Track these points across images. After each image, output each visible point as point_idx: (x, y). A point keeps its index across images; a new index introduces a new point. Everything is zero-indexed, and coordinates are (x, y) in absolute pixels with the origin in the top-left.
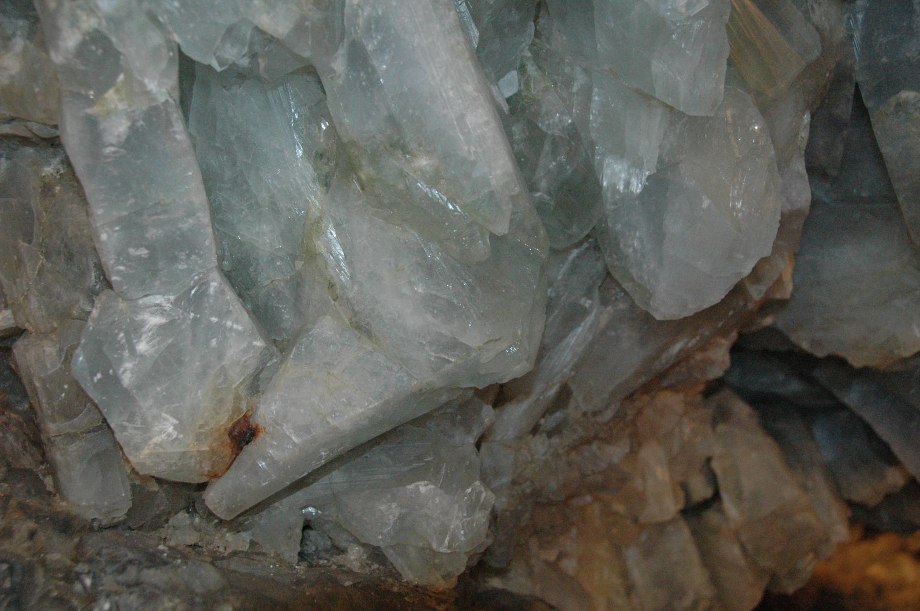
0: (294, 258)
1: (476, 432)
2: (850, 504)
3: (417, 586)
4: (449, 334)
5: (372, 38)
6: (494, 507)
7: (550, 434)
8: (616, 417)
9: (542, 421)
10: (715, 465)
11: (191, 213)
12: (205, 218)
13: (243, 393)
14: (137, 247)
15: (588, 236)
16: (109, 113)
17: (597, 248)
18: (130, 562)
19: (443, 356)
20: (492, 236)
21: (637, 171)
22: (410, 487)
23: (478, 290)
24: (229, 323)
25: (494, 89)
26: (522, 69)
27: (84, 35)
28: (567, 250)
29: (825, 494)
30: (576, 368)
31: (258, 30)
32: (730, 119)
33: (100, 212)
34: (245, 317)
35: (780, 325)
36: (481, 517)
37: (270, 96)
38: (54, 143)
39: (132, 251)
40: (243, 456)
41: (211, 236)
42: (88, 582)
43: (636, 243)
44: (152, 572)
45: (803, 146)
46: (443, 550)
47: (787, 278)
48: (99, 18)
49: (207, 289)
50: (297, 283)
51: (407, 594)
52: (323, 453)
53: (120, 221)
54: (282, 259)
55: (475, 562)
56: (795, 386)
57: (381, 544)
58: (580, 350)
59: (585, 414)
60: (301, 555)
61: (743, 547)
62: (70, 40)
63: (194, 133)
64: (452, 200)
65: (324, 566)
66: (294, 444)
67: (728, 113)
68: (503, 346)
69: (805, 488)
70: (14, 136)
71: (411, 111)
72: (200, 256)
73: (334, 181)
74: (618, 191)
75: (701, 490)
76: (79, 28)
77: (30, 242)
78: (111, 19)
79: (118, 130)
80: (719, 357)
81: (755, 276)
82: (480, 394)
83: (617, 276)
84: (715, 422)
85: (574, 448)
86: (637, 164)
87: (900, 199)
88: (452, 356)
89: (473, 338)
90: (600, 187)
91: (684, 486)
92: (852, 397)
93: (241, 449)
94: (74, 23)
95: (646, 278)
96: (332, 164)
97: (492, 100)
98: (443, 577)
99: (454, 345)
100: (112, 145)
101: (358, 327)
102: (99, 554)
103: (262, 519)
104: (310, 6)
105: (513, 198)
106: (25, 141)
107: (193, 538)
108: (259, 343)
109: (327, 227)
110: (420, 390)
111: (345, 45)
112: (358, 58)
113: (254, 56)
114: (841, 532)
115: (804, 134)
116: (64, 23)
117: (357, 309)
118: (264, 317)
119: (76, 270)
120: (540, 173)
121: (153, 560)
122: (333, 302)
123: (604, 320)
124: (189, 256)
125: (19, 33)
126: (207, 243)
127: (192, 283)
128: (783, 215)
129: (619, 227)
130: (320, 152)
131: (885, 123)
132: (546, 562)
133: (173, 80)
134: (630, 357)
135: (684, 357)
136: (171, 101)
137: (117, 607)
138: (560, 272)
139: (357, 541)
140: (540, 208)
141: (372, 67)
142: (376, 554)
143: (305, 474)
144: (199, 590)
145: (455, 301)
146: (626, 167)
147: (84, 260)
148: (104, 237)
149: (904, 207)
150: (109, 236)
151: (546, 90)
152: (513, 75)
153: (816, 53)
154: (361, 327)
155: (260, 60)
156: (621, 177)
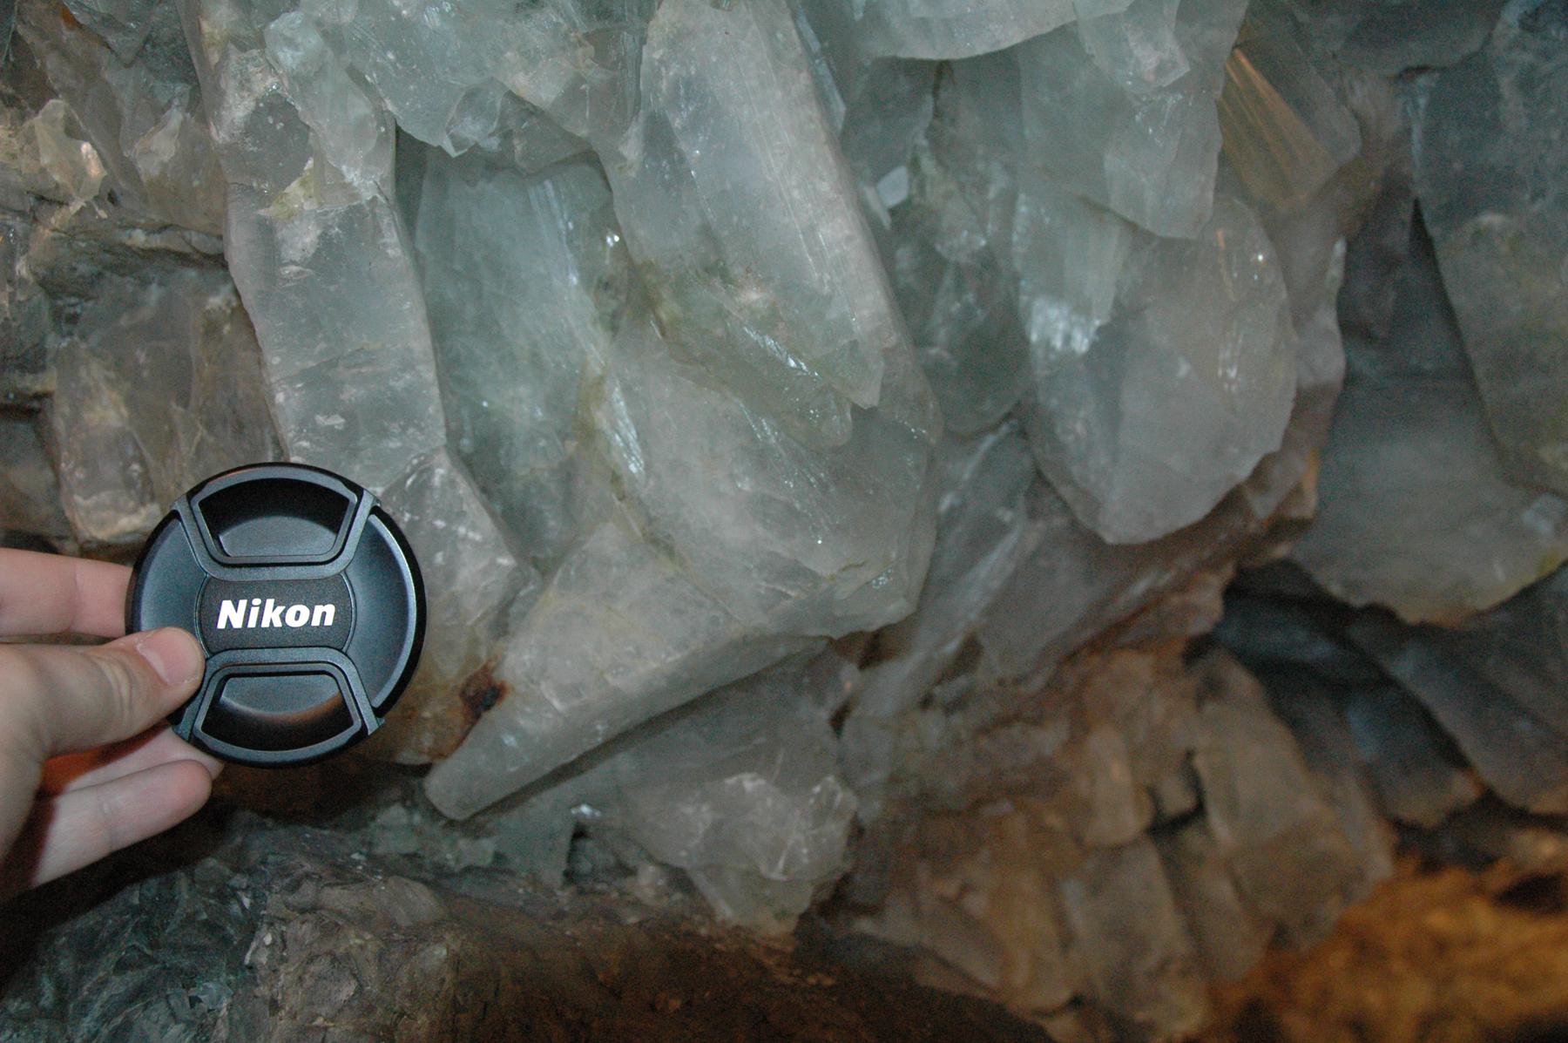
0: (564, 436)
1: (833, 702)
2: (1398, 825)
3: (738, 927)
4: (786, 554)
5: (680, 110)
6: (856, 816)
7: (950, 708)
8: (1048, 686)
9: (937, 690)
10: (1200, 762)
11: (408, 365)
12: (429, 373)
13: (482, 633)
14: (328, 414)
15: (1009, 416)
16: (291, 215)
17: (1023, 433)
18: (307, 876)
19: (779, 587)
20: (856, 409)
21: (1083, 320)
22: (731, 781)
23: (832, 489)
24: (462, 530)
25: (870, 194)
26: (915, 166)
27: (257, 101)
28: (979, 434)
29: (1360, 806)
30: (990, 611)
31: (513, 97)
32: (1222, 244)
33: (276, 360)
34: (486, 522)
35: (1299, 557)
36: (836, 830)
37: (532, 194)
38: (219, 261)
39: (320, 419)
40: (481, 726)
41: (437, 400)
42: (247, 902)
43: (1079, 427)
44: (337, 891)
45: (1335, 288)
46: (776, 875)
47: (1309, 486)
48: (280, 77)
49: (429, 478)
50: (568, 474)
51: (720, 940)
52: (599, 727)
53: (304, 375)
54: (547, 437)
55: (825, 895)
56: (1321, 650)
57: (685, 864)
58: (996, 584)
59: (1001, 682)
60: (570, 876)
61: (1236, 884)
62: (238, 109)
63: (422, 247)
64: (797, 355)
65: (601, 893)
66: (557, 713)
67: (1220, 234)
68: (867, 574)
69: (1330, 800)
70: (168, 252)
71: (735, 219)
72: (421, 430)
73: (624, 322)
74: (1053, 349)
75: (1177, 799)
76: (249, 90)
77: (186, 406)
78: (295, 78)
79: (303, 239)
80: (1206, 604)
81: (1259, 477)
82: (842, 646)
83: (1050, 476)
84: (1200, 701)
85: (984, 730)
86: (1082, 309)
87: (1480, 372)
88: (792, 588)
89: (824, 557)
90: (1025, 339)
91: (1153, 794)
92: (1405, 667)
93: (478, 716)
94: (245, 84)
95: (1093, 478)
96: (622, 298)
97: (863, 208)
98: (777, 916)
99: (795, 572)
100: (294, 263)
101: (655, 542)
102: (264, 863)
103: (511, 820)
104: (589, 62)
105: (887, 353)
106: (183, 259)
107: (411, 845)
108: (506, 561)
109: (612, 391)
110: (745, 637)
111: (641, 119)
112: (659, 138)
113: (507, 135)
114: (1381, 865)
115: (1336, 272)
116: (230, 85)
117: (653, 513)
118: (517, 524)
119: (247, 446)
120: (937, 319)
121: (341, 874)
122: (618, 503)
123: (1032, 541)
124: (404, 429)
125: (176, 102)
126: (431, 410)
127: (408, 470)
128: (1299, 391)
129: (1054, 402)
130: (605, 279)
131: (1458, 261)
132: (944, 900)
133: (385, 168)
134: (1069, 600)
135: (1153, 601)
136: (381, 199)
137: (284, 941)
138: (966, 470)
139: (650, 858)
140: (934, 372)
141: (680, 153)
142: (680, 880)
143: (574, 757)
144: (404, 922)
145: (798, 506)
146: (1066, 312)
147: (258, 432)
148: (280, 397)
149: (1484, 386)
150: (287, 398)
151: (948, 196)
152: (900, 174)
153: (1354, 150)
154: (658, 541)
155: (516, 142)
156: (1058, 328)
